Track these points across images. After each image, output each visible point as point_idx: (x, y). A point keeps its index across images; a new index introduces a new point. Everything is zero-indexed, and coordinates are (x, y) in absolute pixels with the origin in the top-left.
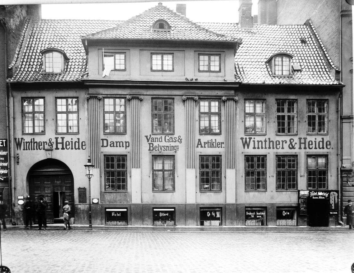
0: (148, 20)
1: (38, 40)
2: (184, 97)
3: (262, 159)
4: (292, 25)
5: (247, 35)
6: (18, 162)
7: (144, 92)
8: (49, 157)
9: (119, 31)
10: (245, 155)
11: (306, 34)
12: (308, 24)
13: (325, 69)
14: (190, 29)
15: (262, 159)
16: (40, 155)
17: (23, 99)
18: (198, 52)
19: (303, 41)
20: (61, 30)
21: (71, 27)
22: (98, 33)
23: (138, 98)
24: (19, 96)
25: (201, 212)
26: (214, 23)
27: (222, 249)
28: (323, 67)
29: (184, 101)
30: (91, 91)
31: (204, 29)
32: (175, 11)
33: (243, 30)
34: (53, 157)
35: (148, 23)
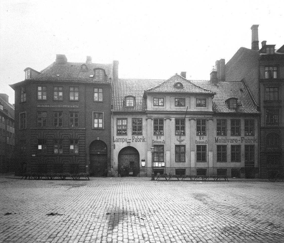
0: (172, 82)
1: (119, 90)
2: (190, 118)
3: (225, 147)
4: (235, 82)
5: (215, 87)
6: (115, 148)
7: (172, 116)
8: (129, 146)
9: (160, 88)
10: (217, 145)
11: (243, 87)
12: (242, 81)
13: (252, 105)
14: (191, 86)
15: (225, 147)
16: (125, 145)
17: (118, 119)
18: (196, 98)
19: (241, 90)
20: (129, 84)
21: (133, 83)
22: (151, 89)
23: (169, 119)
24: (116, 117)
25: (232, 171)
26: (199, 81)
27: (42, 218)
28: (251, 104)
29: (190, 120)
30: (149, 115)
31: (198, 87)
32: (180, 75)
33: (213, 85)
34: (131, 146)
35: (172, 83)
